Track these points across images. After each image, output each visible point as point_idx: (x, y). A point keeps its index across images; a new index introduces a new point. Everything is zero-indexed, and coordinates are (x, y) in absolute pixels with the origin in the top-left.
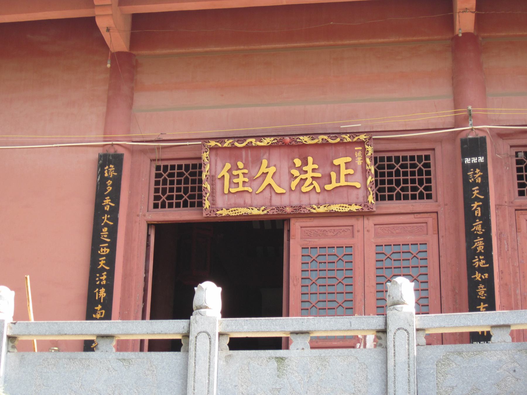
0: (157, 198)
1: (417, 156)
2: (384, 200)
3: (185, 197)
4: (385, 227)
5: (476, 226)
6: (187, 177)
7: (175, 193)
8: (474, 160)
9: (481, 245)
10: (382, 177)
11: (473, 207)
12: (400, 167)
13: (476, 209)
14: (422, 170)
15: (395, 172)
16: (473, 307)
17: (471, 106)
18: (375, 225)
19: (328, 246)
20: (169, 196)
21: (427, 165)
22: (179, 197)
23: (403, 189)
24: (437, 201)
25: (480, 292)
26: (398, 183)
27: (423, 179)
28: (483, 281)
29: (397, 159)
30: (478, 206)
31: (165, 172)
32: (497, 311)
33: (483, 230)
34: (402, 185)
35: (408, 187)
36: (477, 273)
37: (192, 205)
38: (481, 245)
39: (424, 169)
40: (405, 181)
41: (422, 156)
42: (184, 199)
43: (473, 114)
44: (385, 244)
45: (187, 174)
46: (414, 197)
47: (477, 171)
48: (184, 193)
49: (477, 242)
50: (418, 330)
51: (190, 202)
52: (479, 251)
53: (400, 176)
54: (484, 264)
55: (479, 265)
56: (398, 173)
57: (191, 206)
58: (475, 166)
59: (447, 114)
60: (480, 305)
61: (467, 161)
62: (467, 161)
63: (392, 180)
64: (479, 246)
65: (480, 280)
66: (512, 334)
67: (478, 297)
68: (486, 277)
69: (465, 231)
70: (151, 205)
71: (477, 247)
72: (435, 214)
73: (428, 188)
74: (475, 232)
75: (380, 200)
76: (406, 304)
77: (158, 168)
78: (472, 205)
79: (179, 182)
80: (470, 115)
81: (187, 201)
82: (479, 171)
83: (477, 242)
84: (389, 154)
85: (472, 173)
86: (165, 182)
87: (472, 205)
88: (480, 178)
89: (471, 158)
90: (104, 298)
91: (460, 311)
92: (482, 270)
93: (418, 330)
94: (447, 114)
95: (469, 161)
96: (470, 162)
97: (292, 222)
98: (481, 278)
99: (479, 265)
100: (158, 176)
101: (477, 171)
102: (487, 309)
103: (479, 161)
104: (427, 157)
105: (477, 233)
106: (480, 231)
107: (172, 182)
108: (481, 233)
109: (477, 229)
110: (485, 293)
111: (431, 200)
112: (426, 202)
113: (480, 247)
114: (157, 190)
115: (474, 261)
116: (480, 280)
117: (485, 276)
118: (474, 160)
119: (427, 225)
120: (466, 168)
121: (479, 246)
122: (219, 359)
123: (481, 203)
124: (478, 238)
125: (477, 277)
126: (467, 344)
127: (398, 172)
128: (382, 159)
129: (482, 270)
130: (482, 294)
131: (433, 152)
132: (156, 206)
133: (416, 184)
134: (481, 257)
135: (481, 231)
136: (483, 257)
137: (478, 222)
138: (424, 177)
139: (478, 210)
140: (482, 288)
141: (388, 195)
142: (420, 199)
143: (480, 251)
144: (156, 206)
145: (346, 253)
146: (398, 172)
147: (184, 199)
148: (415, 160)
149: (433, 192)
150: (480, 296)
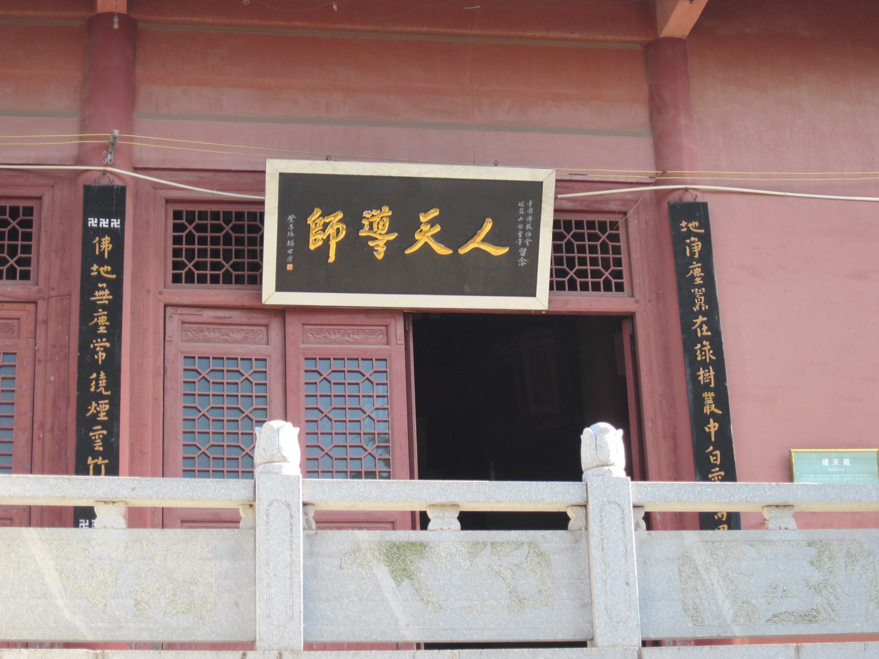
0: (176, 265)
2: (586, 291)
4: (367, 330)
6: (223, 229)
8: (104, 223)
10: (226, 245)
12: (186, 228)
14: (194, 236)
15: (565, 244)
16: (703, 472)
17: (118, 131)
18: (183, 323)
19: (242, 357)
21: (615, 238)
24: (37, 284)
27: (193, 250)
32: (737, 483)
34: (19, 255)
35: (206, 262)
37: (239, 280)
39: (197, 234)
40: (582, 261)
41: (194, 212)
43: (118, 143)
44: (257, 357)
45: (604, 237)
46: (596, 287)
50: (635, 507)
53: (22, 240)
56: (227, 240)
57: (237, 283)
58: (101, 232)
59: (71, 139)
61: (92, 222)
62: (92, 222)
63: (181, 249)
66: (798, 516)
69: (682, 347)
72: (169, 309)
73: (618, 275)
76: (288, 462)
77: (177, 215)
79: (581, 249)
80: (113, 144)
81: (565, 277)
90: (716, 432)
91: (67, 473)
93: (635, 507)
94: (141, 140)
95: (114, 222)
96: (107, 226)
100: (177, 228)
102: (724, 479)
103: (101, 226)
104: (29, 211)
111: (244, 285)
112: (592, 296)
114: (177, 253)
118: (104, 223)
119: (387, 329)
120: (90, 234)
126: (696, 531)
127: (227, 237)
128: (568, 225)
131: (38, 202)
132: (176, 279)
133: (219, 257)
138: (20, 243)
142: (8, 278)
144: (176, 279)
145: (257, 369)
146: (227, 237)
149: (32, 268)
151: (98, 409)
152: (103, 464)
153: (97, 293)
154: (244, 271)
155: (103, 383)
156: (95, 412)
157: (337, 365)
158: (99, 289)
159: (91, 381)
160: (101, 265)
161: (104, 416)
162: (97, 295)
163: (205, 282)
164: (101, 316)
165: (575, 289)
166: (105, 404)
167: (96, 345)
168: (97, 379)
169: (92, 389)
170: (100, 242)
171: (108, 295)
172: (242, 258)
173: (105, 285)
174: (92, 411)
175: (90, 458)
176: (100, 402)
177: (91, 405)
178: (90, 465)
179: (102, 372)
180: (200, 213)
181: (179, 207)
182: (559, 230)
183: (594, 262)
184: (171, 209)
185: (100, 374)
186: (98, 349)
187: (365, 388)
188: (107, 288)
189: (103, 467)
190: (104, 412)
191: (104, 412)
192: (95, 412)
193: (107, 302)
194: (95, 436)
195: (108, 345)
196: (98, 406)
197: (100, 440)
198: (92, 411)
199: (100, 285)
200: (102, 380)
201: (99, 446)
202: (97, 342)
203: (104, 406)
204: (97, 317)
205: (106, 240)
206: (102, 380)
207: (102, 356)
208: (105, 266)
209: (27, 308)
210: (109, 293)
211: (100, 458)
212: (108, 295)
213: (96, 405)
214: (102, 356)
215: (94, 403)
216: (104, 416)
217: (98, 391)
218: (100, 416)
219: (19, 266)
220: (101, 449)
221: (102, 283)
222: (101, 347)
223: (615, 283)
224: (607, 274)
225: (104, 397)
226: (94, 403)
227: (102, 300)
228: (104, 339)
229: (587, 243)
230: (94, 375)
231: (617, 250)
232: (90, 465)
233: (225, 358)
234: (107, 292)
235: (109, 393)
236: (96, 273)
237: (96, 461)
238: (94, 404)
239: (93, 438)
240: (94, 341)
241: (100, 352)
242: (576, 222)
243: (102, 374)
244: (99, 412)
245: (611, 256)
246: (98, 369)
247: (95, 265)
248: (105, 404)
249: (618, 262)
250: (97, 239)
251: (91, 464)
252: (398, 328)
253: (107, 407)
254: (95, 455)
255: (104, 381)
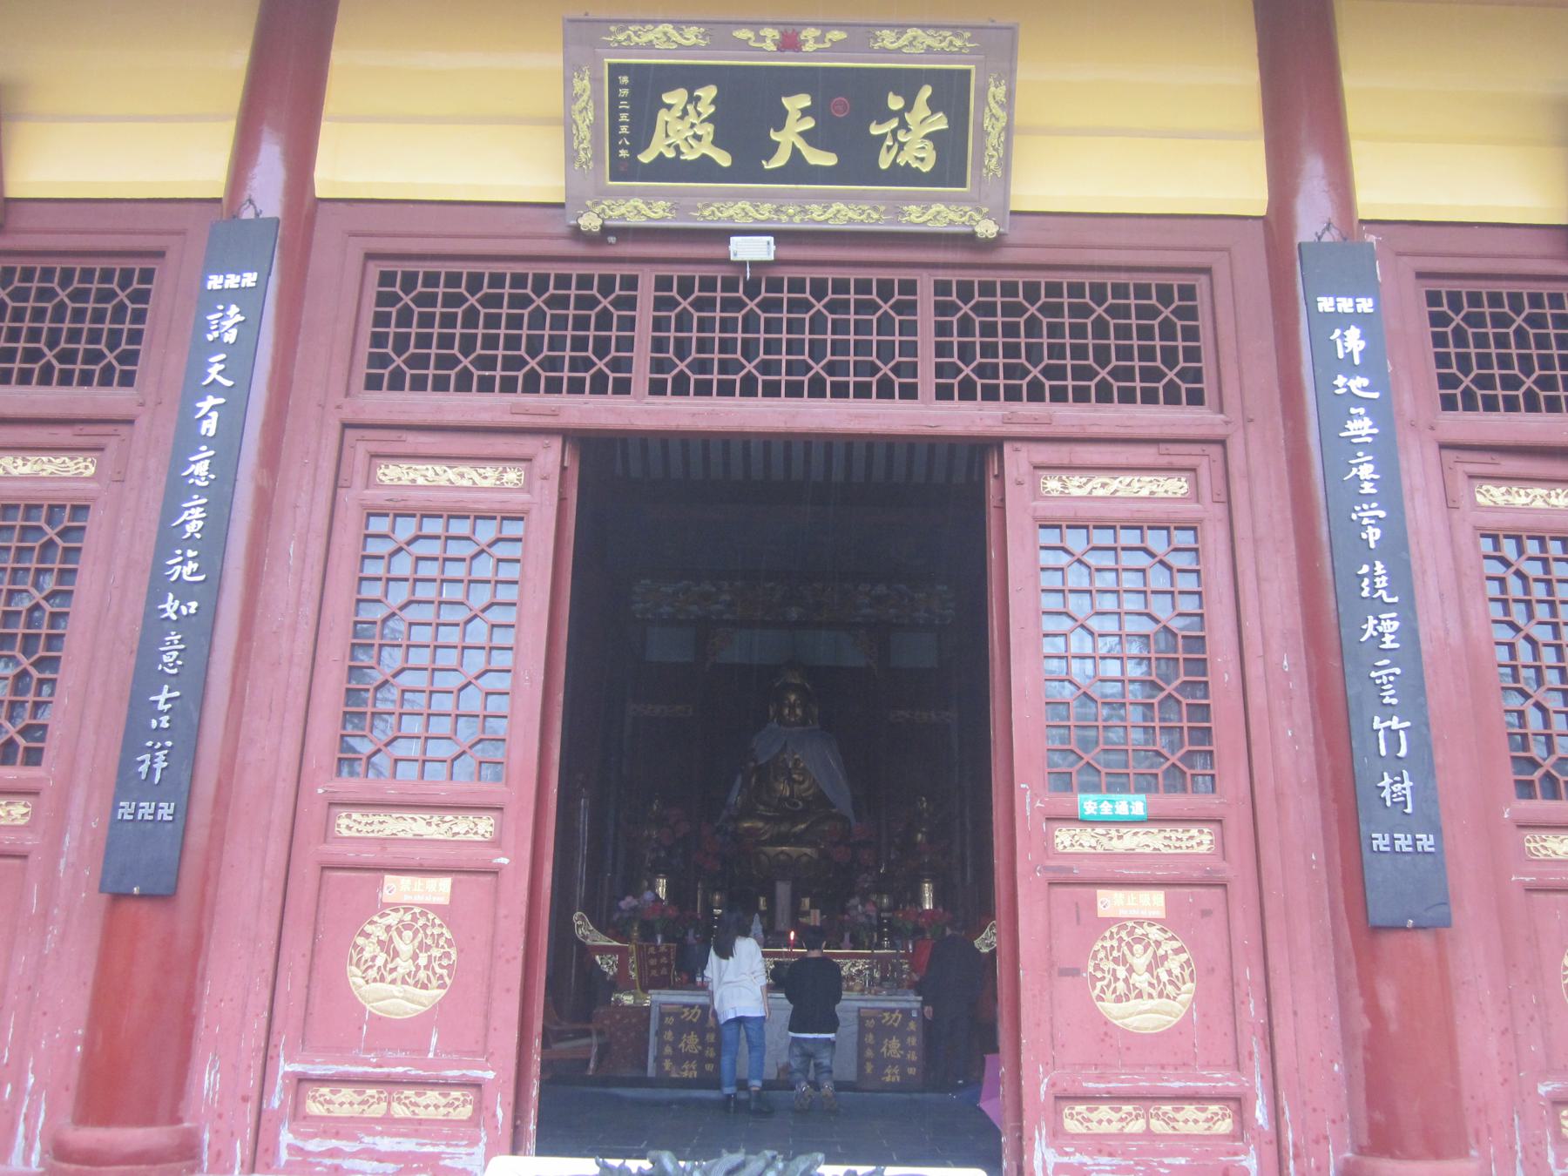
0: (1446, 381)
1: (1091, 285)
3: (1035, 372)
5: (195, 462)
7: (82, 346)
8: (1345, 305)
9: (197, 519)
11: (200, 409)
13: (205, 417)
20: (414, 357)
22: (511, 363)
23: (981, 371)
25: (168, 654)
26: (1033, 353)
28: (182, 622)
29: (1098, 292)
30: (213, 408)
31: (64, 285)
33: (212, 477)
36: (171, 596)
38: (197, 519)
40: (446, 341)
42: (527, 368)
47: (234, 309)
48: (528, 352)
49: (189, 508)
51: (832, 383)
52: (188, 535)
54: (192, 574)
55: (181, 574)
60: (159, 692)
64: (191, 521)
65: (174, 617)
67: (160, 667)
68: (192, 611)
70: (359, 380)
71: (186, 522)
74: (191, 481)
75: (855, 397)
78: (199, 405)
82: (238, 310)
83: (189, 508)
84: (455, 267)
85: (220, 315)
86: (405, 318)
87: (199, 405)
88: (234, 332)
89: (1355, 297)
92: (184, 590)
97: (1007, 448)
98: (178, 612)
99: (181, 574)
101: (234, 309)
105: (194, 483)
106: (203, 479)
107: (492, 321)
108: (206, 483)
109: (196, 473)
110: (178, 658)
113: (194, 522)
115: (170, 562)
116: (174, 617)
117: (188, 608)
118: (1345, 305)
121: (191, 521)
122: (1036, 794)
123: (222, 401)
124: (196, 497)
125: (169, 609)
129: (184, 590)
130: (172, 660)
134: (191, 553)
135: (207, 478)
136: (195, 553)
137: (206, 452)
139: (210, 418)
140: (176, 642)
141: (787, 382)
142: (458, 389)
143: (192, 534)
147: (527, 368)
148: (1083, 296)
150: (166, 665)
151: (1380, 629)
152: (1402, 729)
153: (1350, 425)
154: (849, 376)
155: (1382, 582)
156: (1375, 634)
157: (1103, 538)
158: (1351, 417)
159: (1362, 577)
160: (1349, 376)
161: (1392, 641)
162: (1351, 429)
163: (1064, 399)
164: (1362, 463)
165: (1474, 408)
166: (1392, 619)
167: (1361, 514)
168: (1372, 575)
169: (1365, 593)
170: (1343, 337)
171: (1371, 427)
172: (992, 357)
173: (1362, 411)
174: (1370, 631)
175: (1377, 719)
176: (1381, 616)
177: (1366, 621)
178: (1379, 730)
179: (1378, 563)
180: (1115, 287)
181: (389, 266)
182: (803, 296)
183: (424, 341)
184: (375, 269)
185: (1374, 565)
186: (1365, 522)
187: (1077, 577)
188: (1367, 414)
189: (1402, 734)
190: (1390, 634)
191: (1390, 634)
192: (1375, 634)
193: (1369, 440)
194: (1380, 677)
195: (1382, 514)
196: (1379, 624)
197: (1390, 686)
198: (1370, 631)
199: (1353, 411)
200: (1380, 576)
201: (1391, 697)
202: (1363, 510)
203: (1390, 625)
204: (1357, 465)
205: (1353, 333)
206: (1380, 576)
207: (1374, 534)
208: (1358, 378)
209: (1206, 453)
210: (1371, 423)
211: (1395, 719)
212: (1371, 427)
213: (1376, 622)
214: (1373, 535)
215: (1370, 618)
216: (1392, 641)
217: (1375, 596)
218: (1384, 643)
219: (1049, 379)
220: (1394, 701)
221: (1356, 408)
222: (1370, 518)
223: (1119, 388)
224: (399, 361)
225: (1389, 607)
226: (1370, 618)
227: (1360, 436)
228: (1374, 505)
229: (1490, 330)
230: (1365, 569)
231: (1191, 334)
232: (1379, 730)
233: (1091, 524)
234: (1367, 422)
235: (1396, 599)
236: (1344, 390)
237: (1387, 724)
238: (1372, 621)
239: (1378, 682)
240: (1357, 508)
241: (1369, 527)
242: (1181, 287)
243: (1379, 567)
244: (1382, 635)
245: (1452, 350)
246: (1369, 556)
247: (1340, 377)
248: (1392, 619)
249: (1193, 354)
250: (1338, 332)
251: (1379, 730)
252: (550, 455)
253: (1396, 624)
254: (1387, 711)
255: (1384, 578)
